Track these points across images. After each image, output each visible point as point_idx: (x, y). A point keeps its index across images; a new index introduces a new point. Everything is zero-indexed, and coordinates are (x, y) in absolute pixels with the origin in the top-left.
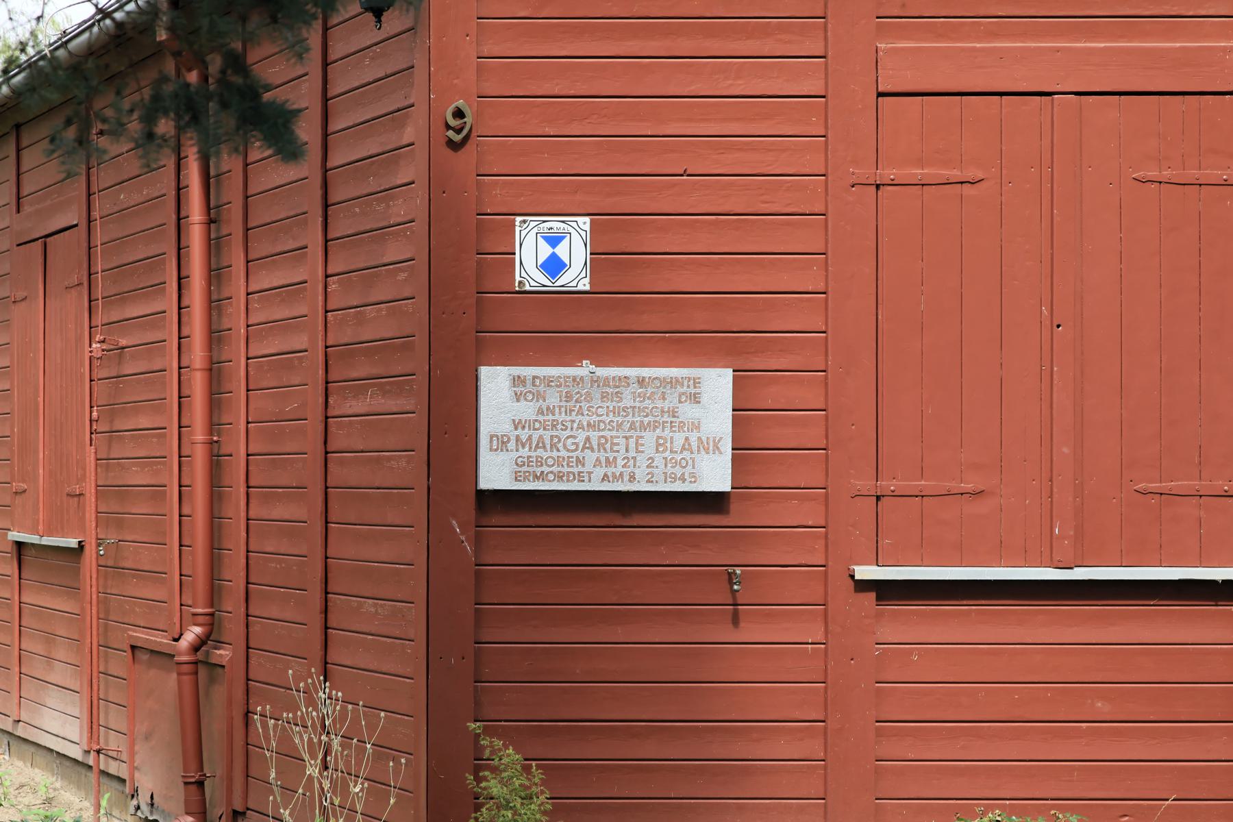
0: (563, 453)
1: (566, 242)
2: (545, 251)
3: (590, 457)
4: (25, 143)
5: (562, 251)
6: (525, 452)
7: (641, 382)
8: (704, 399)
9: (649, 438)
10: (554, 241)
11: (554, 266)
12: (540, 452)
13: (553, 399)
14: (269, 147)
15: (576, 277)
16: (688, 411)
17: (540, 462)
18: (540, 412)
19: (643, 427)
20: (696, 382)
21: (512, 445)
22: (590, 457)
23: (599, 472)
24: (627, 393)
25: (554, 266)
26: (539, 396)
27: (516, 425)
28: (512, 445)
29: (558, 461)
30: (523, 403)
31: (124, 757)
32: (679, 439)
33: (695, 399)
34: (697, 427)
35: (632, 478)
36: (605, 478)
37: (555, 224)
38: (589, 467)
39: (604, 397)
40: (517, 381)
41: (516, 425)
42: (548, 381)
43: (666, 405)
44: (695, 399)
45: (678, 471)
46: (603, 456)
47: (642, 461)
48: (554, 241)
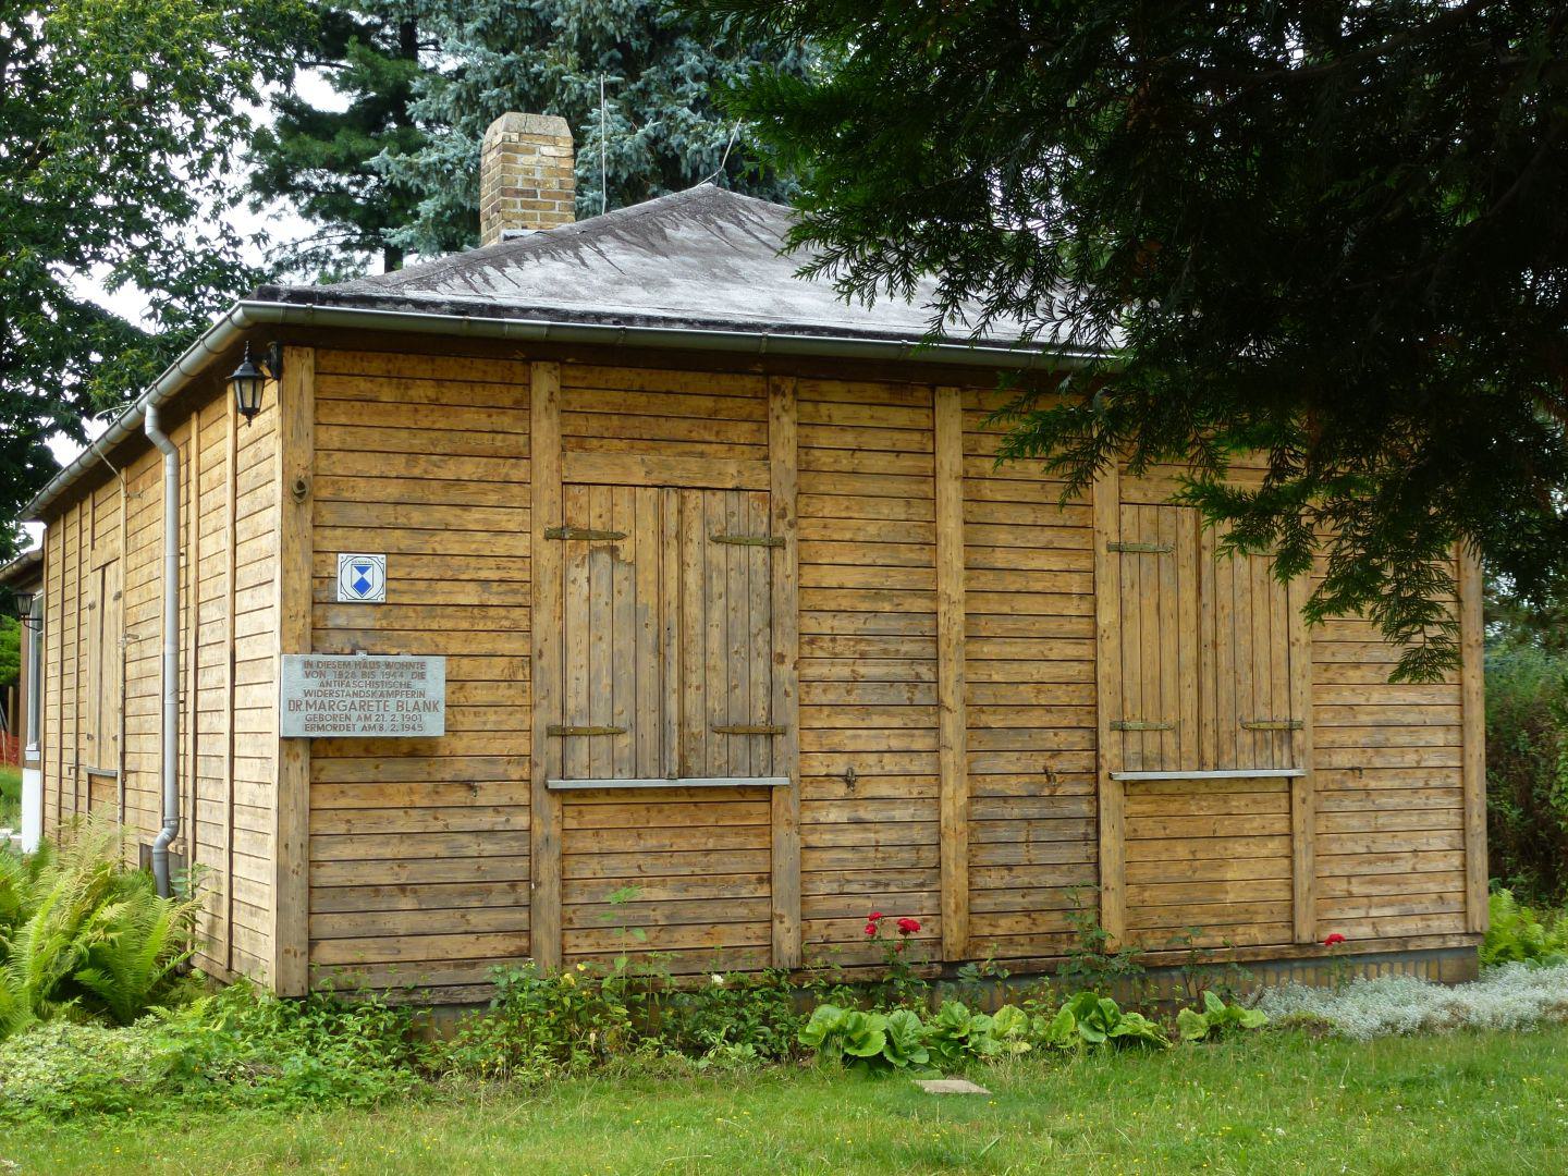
0: (337, 712)
1: (369, 572)
2: (357, 576)
3: (354, 714)
4: (203, 425)
5: (367, 576)
6: (312, 711)
7: (388, 665)
8: (428, 676)
9: (392, 702)
10: (362, 570)
11: (362, 586)
12: (322, 712)
13: (330, 677)
14: (1109, 286)
15: (376, 593)
16: (418, 685)
17: (322, 718)
18: (322, 685)
19: (389, 695)
20: (423, 665)
21: (303, 707)
22: (354, 714)
23: (360, 724)
24: (378, 672)
25: (362, 586)
26: (321, 674)
27: (307, 693)
28: (303, 707)
29: (334, 717)
30: (310, 679)
31: (983, 336)
32: (411, 702)
33: (422, 676)
34: (422, 694)
35: (381, 728)
36: (364, 728)
37: (362, 559)
38: (354, 720)
39: (364, 675)
40: (307, 664)
41: (307, 693)
42: (327, 664)
43: (403, 680)
44: (422, 676)
45: (411, 723)
46: (362, 713)
47: (388, 717)
48: (362, 570)
